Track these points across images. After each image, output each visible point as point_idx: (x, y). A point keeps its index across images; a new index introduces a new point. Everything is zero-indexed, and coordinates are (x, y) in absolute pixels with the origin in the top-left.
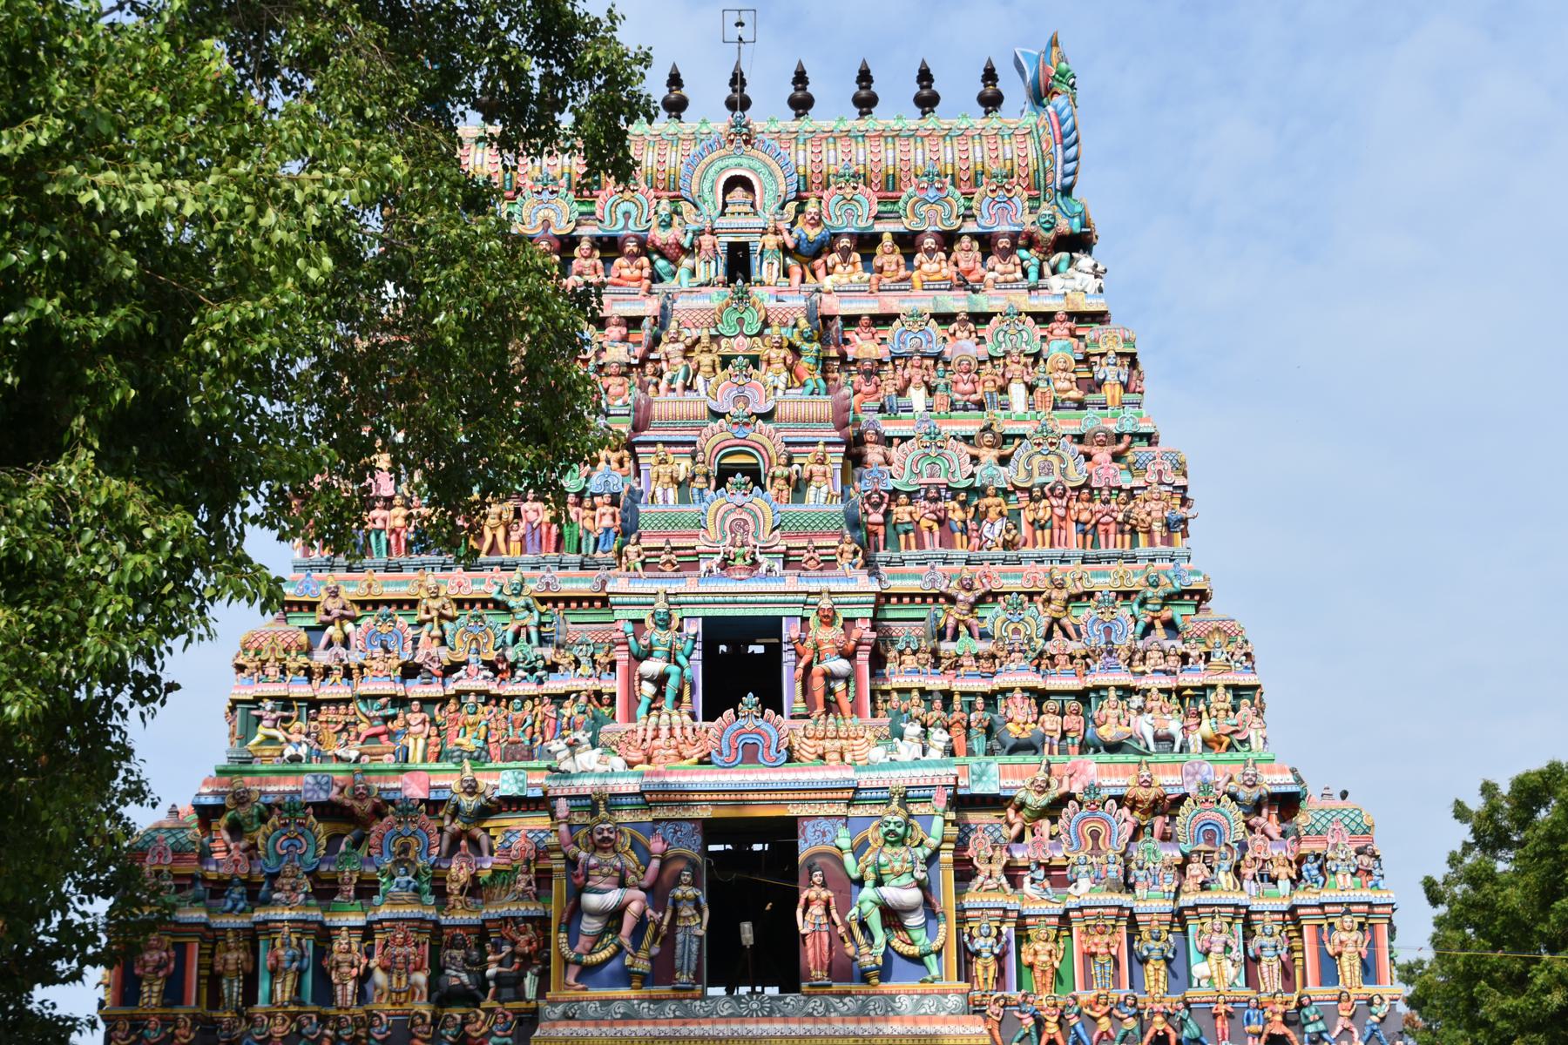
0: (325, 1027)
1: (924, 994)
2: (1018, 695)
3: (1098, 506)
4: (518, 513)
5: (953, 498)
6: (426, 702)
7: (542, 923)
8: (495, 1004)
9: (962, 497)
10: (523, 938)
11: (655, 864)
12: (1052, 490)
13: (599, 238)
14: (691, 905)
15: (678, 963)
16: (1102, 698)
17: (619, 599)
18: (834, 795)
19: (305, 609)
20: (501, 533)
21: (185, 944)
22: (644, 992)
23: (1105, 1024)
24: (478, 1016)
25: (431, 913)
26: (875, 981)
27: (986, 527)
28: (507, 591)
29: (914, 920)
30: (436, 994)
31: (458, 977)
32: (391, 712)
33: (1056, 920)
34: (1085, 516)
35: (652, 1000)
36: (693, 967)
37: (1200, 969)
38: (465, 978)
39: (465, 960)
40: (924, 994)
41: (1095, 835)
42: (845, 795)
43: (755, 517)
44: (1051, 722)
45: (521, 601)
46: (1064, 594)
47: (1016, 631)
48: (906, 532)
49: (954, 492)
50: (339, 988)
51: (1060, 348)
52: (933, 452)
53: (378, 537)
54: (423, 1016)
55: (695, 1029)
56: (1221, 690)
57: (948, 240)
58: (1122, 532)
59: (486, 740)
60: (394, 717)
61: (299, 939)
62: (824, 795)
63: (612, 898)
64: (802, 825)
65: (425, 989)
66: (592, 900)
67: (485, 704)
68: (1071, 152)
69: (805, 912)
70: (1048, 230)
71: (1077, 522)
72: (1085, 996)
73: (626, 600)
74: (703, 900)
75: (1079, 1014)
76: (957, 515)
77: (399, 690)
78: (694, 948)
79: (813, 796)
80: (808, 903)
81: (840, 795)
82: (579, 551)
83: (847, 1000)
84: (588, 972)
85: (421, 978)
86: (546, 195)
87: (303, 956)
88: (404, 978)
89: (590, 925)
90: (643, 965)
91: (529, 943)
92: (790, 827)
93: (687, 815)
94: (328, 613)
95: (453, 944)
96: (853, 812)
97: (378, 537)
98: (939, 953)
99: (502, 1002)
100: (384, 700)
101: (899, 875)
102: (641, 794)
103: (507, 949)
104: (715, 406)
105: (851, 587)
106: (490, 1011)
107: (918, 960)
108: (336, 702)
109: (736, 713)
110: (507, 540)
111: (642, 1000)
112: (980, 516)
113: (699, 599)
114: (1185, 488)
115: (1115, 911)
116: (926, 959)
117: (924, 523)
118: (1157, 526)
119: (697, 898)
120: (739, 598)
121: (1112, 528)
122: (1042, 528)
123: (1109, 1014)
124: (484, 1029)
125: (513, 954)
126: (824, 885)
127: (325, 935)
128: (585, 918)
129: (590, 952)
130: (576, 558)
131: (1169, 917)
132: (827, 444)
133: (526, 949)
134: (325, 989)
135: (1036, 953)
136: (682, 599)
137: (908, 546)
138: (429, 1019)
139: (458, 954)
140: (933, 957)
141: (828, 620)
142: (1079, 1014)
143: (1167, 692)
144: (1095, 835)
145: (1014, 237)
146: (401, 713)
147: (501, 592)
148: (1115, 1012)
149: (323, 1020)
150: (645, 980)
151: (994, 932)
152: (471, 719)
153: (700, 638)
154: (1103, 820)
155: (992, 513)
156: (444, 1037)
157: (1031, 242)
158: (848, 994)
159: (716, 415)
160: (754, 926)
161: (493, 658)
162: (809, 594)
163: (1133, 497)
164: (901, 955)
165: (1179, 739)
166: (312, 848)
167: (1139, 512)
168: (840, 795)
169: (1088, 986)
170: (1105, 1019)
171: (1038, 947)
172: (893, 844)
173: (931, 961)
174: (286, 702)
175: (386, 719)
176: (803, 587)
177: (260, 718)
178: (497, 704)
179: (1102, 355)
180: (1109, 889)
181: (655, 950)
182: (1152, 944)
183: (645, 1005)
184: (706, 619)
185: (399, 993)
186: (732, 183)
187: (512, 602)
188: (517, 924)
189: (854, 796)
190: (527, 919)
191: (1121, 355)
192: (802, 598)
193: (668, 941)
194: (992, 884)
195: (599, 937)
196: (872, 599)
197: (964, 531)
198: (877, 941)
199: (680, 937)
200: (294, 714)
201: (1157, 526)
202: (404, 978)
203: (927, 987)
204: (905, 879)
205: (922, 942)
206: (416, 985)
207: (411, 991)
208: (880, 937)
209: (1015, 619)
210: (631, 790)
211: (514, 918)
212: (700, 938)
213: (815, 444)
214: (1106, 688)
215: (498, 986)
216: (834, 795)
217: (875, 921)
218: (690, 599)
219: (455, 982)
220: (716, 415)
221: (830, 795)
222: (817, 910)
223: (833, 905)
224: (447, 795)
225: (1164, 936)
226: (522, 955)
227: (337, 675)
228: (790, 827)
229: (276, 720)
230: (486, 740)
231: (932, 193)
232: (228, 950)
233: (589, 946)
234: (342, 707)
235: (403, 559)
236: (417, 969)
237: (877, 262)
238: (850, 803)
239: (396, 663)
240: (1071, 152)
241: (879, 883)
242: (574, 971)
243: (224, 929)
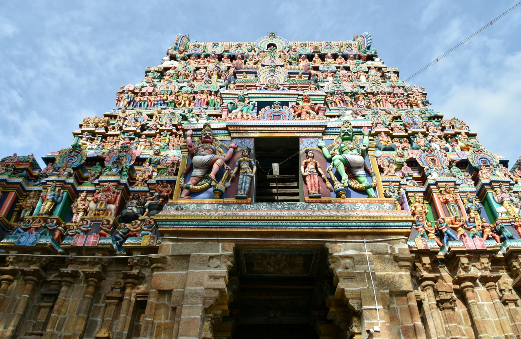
0: (59, 226)
1: (370, 203)
2: (383, 134)
3: (397, 99)
4: (194, 98)
5: (346, 95)
6: (147, 136)
7: (172, 183)
8: (146, 217)
9: (350, 94)
10: (164, 190)
11: (231, 150)
12: (381, 92)
13: (230, 56)
14: (247, 163)
15: (239, 187)
16: (415, 137)
17: (225, 96)
18: (316, 129)
19: (113, 118)
20: (187, 102)
21: (8, 193)
22: (221, 200)
23: (462, 231)
24: (136, 223)
25: (124, 180)
26: (343, 196)
27: (359, 103)
28: (186, 112)
29: (361, 172)
30: (119, 216)
31: (132, 208)
32: (133, 136)
33: (422, 194)
34: (393, 101)
35: (224, 204)
36: (247, 188)
37: (499, 209)
38: (135, 209)
39: (137, 204)
40: (370, 203)
41: (433, 161)
42: (321, 129)
43: (278, 78)
44: (397, 144)
45: (191, 115)
46: (391, 116)
47: (377, 119)
48: (331, 103)
49: (346, 93)
50: (75, 215)
51: (373, 72)
52: (338, 85)
53: (144, 103)
54: (108, 221)
55: (246, 213)
56: (464, 134)
57: (335, 56)
58: (407, 106)
59: (168, 144)
60: (134, 139)
61: (60, 190)
62: (311, 129)
63: (206, 158)
64: (300, 139)
65: (113, 212)
66: (197, 158)
67: (171, 135)
68: (369, 38)
69: (305, 168)
70: (365, 53)
71: (391, 103)
72: (448, 219)
73: (228, 96)
74: (253, 163)
75: (447, 226)
76: (348, 99)
77: (139, 131)
78: (248, 181)
79: (306, 129)
80: (306, 164)
81: (319, 129)
82: (214, 106)
83: (329, 205)
84: (193, 194)
85: (113, 207)
86: (215, 47)
87: (59, 196)
88: (103, 205)
89: (197, 172)
90: (220, 186)
91: (168, 192)
92: (296, 140)
93: (247, 136)
94: (120, 118)
95: (133, 199)
96: (324, 137)
97: (144, 103)
98: (375, 189)
99: (149, 216)
100: (131, 133)
101: (352, 149)
102: (226, 129)
103: (156, 194)
104: (263, 64)
105: (316, 94)
106: (143, 220)
107: (363, 192)
108: (113, 136)
109: (271, 108)
110: (190, 104)
111: (219, 204)
112: (356, 100)
113: (256, 96)
114: (426, 94)
115: (453, 184)
116: (369, 190)
117: (337, 101)
118: (419, 102)
119: (250, 162)
120: (272, 96)
121: (403, 104)
122: (379, 102)
123: (462, 226)
124: (139, 228)
125: (159, 197)
126: (313, 157)
127: (74, 195)
128: (195, 170)
129: (195, 184)
130: (214, 108)
131: (475, 194)
132: (303, 74)
133: (166, 194)
134: (67, 214)
135: (415, 208)
136: (249, 95)
137: (332, 106)
138: (111, 223)
139: (135, 202)
140: (372, 189)
141: (307, 100)
142: (447, 226)
143: (440, 137)
144: (433, 161)
145: (355, 55)
146: (137, 139)
147: (184, 112)
148: (465, 226)
149: (59, 223)
150: (221, 195)
151: (397, 192)
152: (163, 138)
153: (256, 105)
154: (435, 156)
155: (361, 98)
156: (118, 233)
157: (360, 57)
158: (330, 202)
159: (263, 66)
160: (280, 166)
161: (176, 123)
162: (299, 95)
163: (409, 97)
164: (355, 190)
165: (450, 149)
166: (79, 161)
167: (411, 99)
168: (319, 129)
169: (448, 213)
170: (460, 229)
171: (415, 205)
172: (347, 139)
173: (371, 191)
174: (94, 134)
175: (131, 139)
176: (297, 92)
177: (82, 138)
178: (176, 136)
179: (388, 72)
180: (447, 176)
181: (228, 184)
182: (471, 204)
183: (221, 206)
184: (256, 139)
185: (99, 211)
186: (269, 46)
187: (187, 115)
188: (163, 184)
189: (326, 130)
190: (168, 182)
191: (395, 72)
192: (297, 96)
193: (235, 180)
194: (389, 174)
195: (201, 179)
196: (324, 97)
197: (352, 104)
198: (343, 178)
199: (241, 177)
200: (96, 138)
201: (419, 102)
202: (103, 205)
203: (372, 199)
204: (355, 151)
205: (365, 181)
206: (110, 210)
207: (106, 211)
208: (345, 176)
209: (377, 116)
210: (222, 127)
211: (162, 181)
212: (252, 177)
213: (298, 73)
214: (417, 133)
215: (150, 210)
216: (316, 129)
217: (342, 169)
218: (253, 95)
219: (130, 211)
220: (263, 66)
221: (314, 129)
222: (311, 166)
223: (318, 165)
224: (147, 156)
225: (474, 201)
226: (163, 197)
227: (116, 129)
228: (296, 140)
229: (88, 138)
230: (168, 144)
231: (329, 47)
232: (30, 198)
233: (194, 181)
234: (115, 137)
235: (152, 107)
236: (109, 202)
237: (314, 59)
238: (324, 133)
239: (139, 124)
240: (369, 38)
241: (341, 152)
242: (186, 191)
243: (31, 191)
